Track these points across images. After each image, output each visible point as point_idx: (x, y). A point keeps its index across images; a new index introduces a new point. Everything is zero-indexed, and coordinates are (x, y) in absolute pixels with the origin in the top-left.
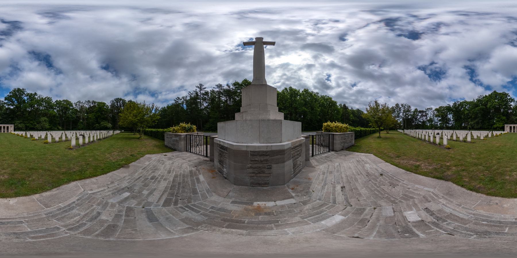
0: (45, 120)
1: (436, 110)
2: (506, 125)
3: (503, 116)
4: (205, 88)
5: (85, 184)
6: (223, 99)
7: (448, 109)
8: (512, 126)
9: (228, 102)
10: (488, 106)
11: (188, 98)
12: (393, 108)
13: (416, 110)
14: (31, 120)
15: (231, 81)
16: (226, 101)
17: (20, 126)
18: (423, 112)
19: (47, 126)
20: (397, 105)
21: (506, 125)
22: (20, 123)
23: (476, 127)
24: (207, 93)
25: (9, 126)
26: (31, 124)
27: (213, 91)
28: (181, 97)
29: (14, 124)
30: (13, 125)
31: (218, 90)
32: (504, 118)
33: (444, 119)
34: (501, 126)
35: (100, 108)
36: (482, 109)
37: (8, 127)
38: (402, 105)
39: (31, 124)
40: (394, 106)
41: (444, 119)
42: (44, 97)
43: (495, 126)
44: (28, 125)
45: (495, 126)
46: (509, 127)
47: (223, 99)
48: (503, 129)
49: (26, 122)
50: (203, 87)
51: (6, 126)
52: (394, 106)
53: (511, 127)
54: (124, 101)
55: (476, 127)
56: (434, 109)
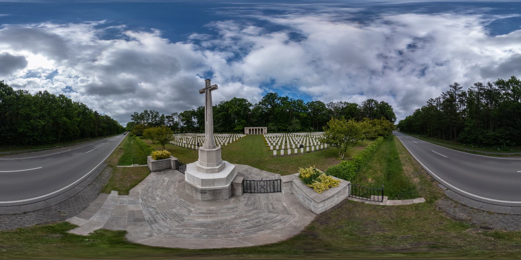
0: (296, 122)
1: (181, 114)
2: (245, 128)
3: (243, 119)
4: (461, 88)
5: (363, 203)
6: (484, 101)
7: (193, 113)
8: (251, 128)
9: (489, 106)
10: (229, 112)
11: (442, 100)
12: (142, 114)
13: (163, 115)
14: (284, 123)
15: (492, 80)
16: (487, 104)
17: (272, 128)
18: (169, 117)
19: (299, 127)
20: (146, 112)
21: (245, 128)
22: (273, 126)
23: (219, 130)
24: (464, 94)
25: (263, 128)
26: (283, 126)
27: (471, 92)
28: (434, 99)
29: (267, 126)
30: (266, 128)
31: (476, 90)
32: (244, 121)
33: (189, 122)
34: (241, 129)
35: (351, 110)
36: (224, 115)
37: (262, 130)
38: (151, 112)
39: (283, 126)
40: (143, 112)
41: (189, 122)
42: (296, 100)
43: (235, 129)
44: (280, 127)
45: (235, 129)
46: (248, 130)
47: (484, 101)
48: (243, 131)
49: (278, 124)
50: (459, 87)
51: (260, 128)
52: (143, 112)
53: (250, 130)
54: (376, 103)
55: (219, 130)
56: (179, 114)
